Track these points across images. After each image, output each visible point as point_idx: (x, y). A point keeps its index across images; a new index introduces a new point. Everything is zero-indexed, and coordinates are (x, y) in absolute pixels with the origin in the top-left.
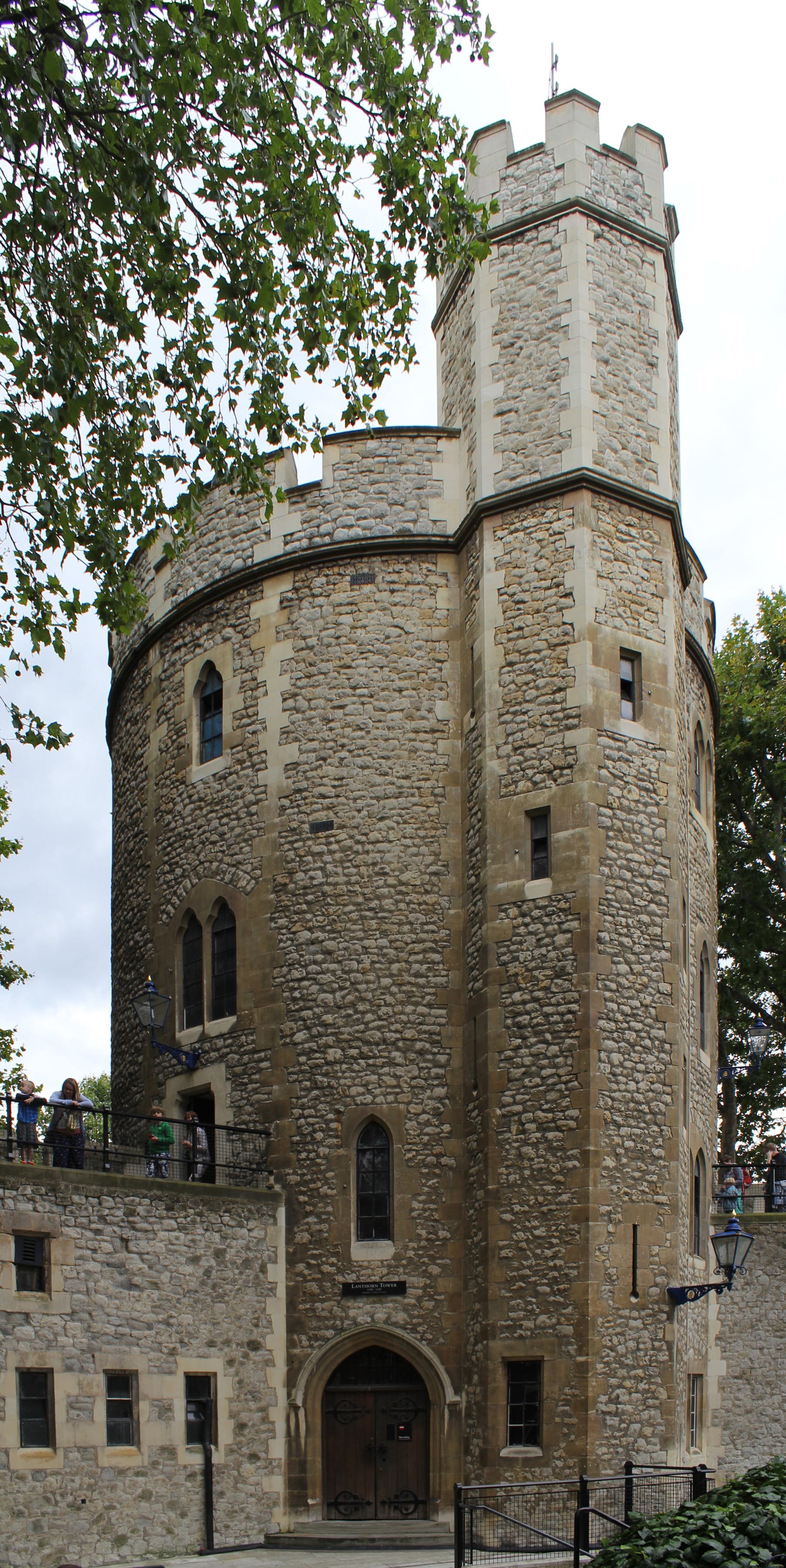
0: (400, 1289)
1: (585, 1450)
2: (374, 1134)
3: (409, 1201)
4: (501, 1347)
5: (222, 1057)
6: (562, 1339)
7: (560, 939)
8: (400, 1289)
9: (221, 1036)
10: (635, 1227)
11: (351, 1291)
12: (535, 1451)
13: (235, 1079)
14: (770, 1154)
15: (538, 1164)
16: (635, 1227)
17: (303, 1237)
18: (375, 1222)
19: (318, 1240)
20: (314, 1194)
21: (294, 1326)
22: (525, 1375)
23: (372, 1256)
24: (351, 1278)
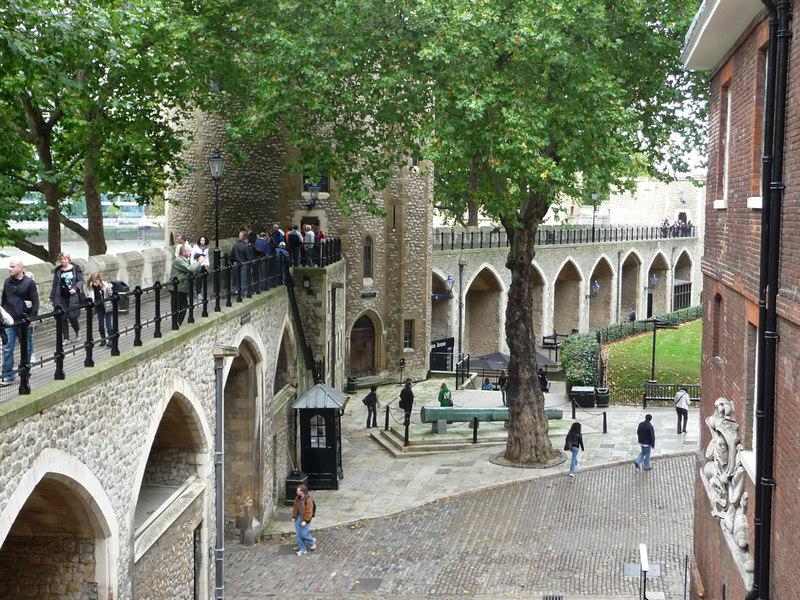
0: (374, 295)
1: (203, 111)
2: (369, 239)
3: (378, 265)
4: (405, 316)
5: (324, 208)
6: (419, 313)
7: (421, 187)
8: (374, 295)
9: (323, 200)
10: (605, 431)
11: (364, 296)
12: (412, 350)
13: (330, 217)
14: (162, 25)
15: (414, 257)
16: (605, 431)
17: (350, 277)
18: (368, 273)
19: (355, 278)
20: (354, 261)
21: (348, 309)
22: (410, 323)
23: (368, 282)
24: (363, 292)
